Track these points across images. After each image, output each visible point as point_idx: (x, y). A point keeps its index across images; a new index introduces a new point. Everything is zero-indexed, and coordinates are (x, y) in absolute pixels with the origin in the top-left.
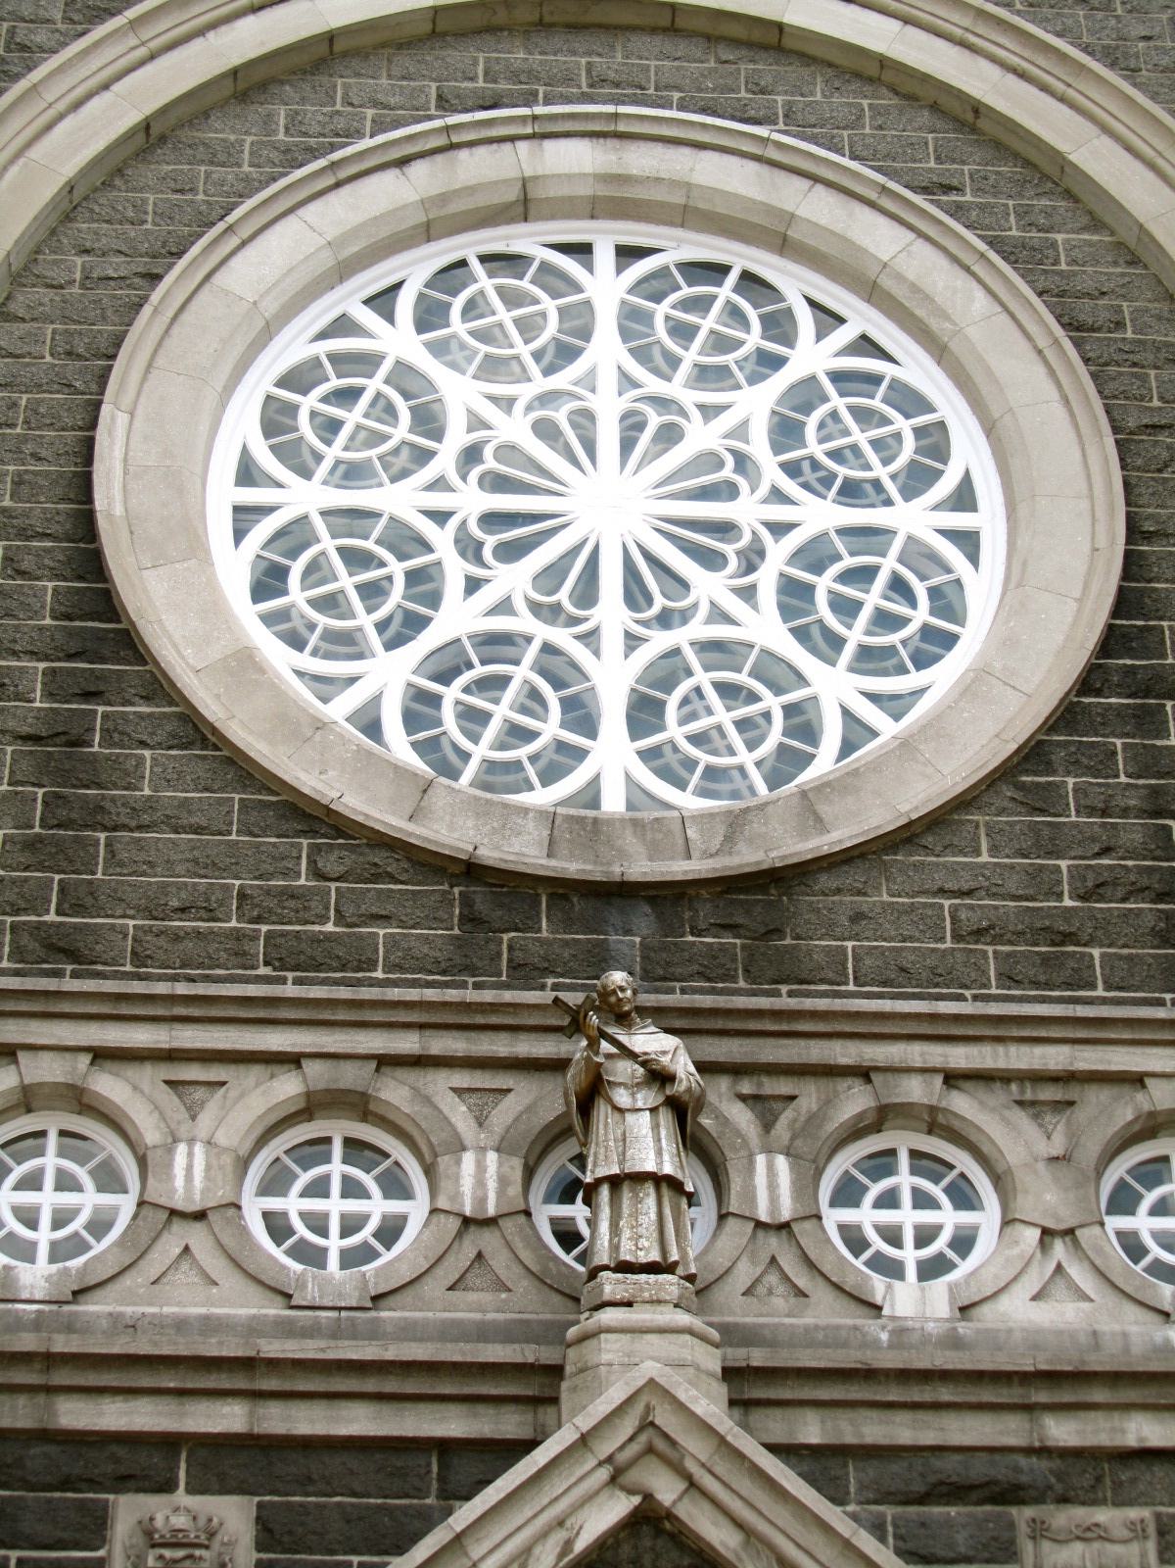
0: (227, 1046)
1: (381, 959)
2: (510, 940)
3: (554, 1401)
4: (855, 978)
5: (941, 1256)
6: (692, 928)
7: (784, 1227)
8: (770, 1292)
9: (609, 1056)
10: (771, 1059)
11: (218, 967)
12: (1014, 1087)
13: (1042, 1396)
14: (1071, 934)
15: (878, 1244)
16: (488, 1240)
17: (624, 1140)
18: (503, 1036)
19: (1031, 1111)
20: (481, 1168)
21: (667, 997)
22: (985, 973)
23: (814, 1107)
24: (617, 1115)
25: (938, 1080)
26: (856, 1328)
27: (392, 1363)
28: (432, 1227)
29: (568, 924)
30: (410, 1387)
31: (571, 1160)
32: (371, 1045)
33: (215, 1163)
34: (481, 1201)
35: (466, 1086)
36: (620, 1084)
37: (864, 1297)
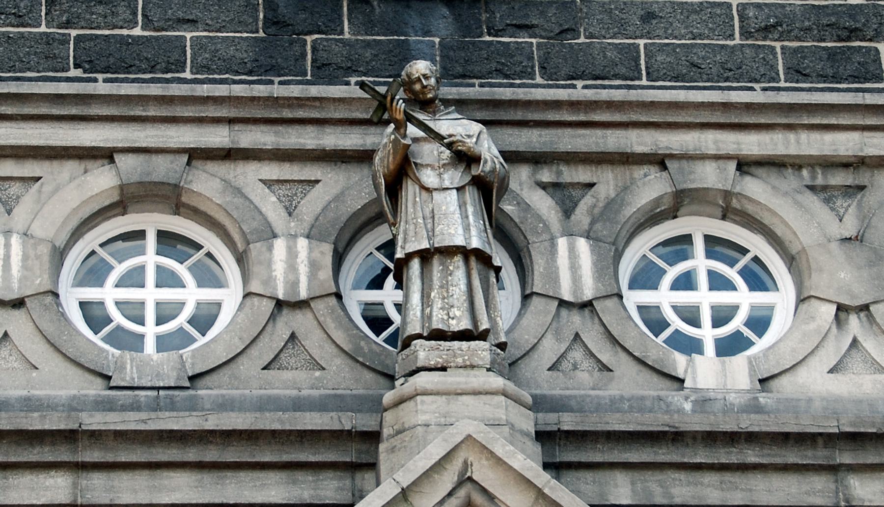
0: (41, 142)
1: (189, 61)
2: (314, 42)
3: (373, 466)
4: (648, 74)
5: (738, 334)
6: (488, 29)
7: (587, 305)
8: (575, 367)
9: (416, 140)
10: (569, 148)
11: (29, 70)
12: (805, 172)
13: (846, 458)
14: (856, 29)
15: (677, 323)
16: (300, 321)
17: (433, 217)
18: (310, 129)
19: (822, 196)
20: (292, 254)
21: (468, 90)
22: (773, 68)
23: (613, 194)
24: (425, 194)
25: (732, 166)
26: (660, 399)
27: (212, 432)
28: (247, 309)
29: (369, 26)
30: (231, 455)
31: (378, 249)
32: (182, 139)
33: (32, 253)
34: (294, 285)
35: (275, 178)
36: (427, 165)
37: (666, 371)
